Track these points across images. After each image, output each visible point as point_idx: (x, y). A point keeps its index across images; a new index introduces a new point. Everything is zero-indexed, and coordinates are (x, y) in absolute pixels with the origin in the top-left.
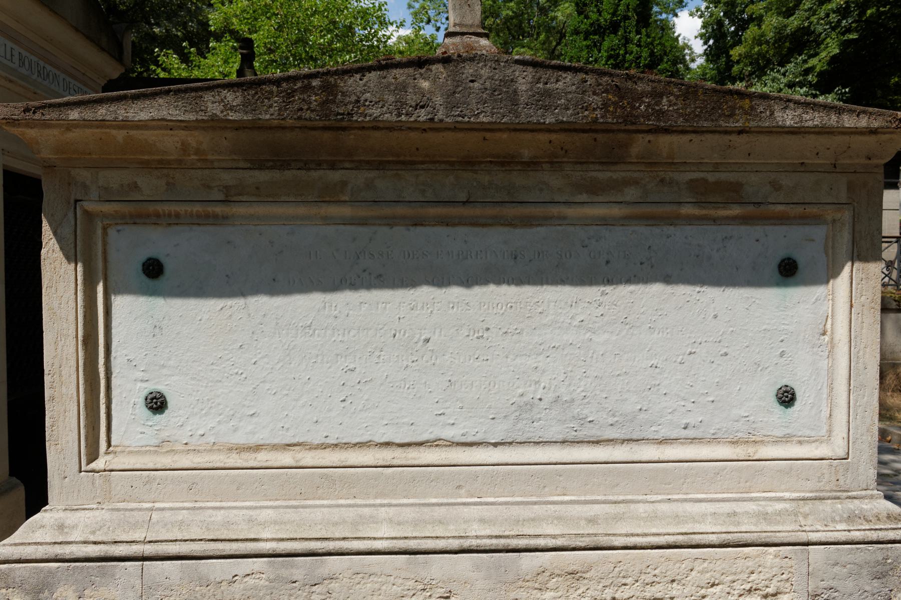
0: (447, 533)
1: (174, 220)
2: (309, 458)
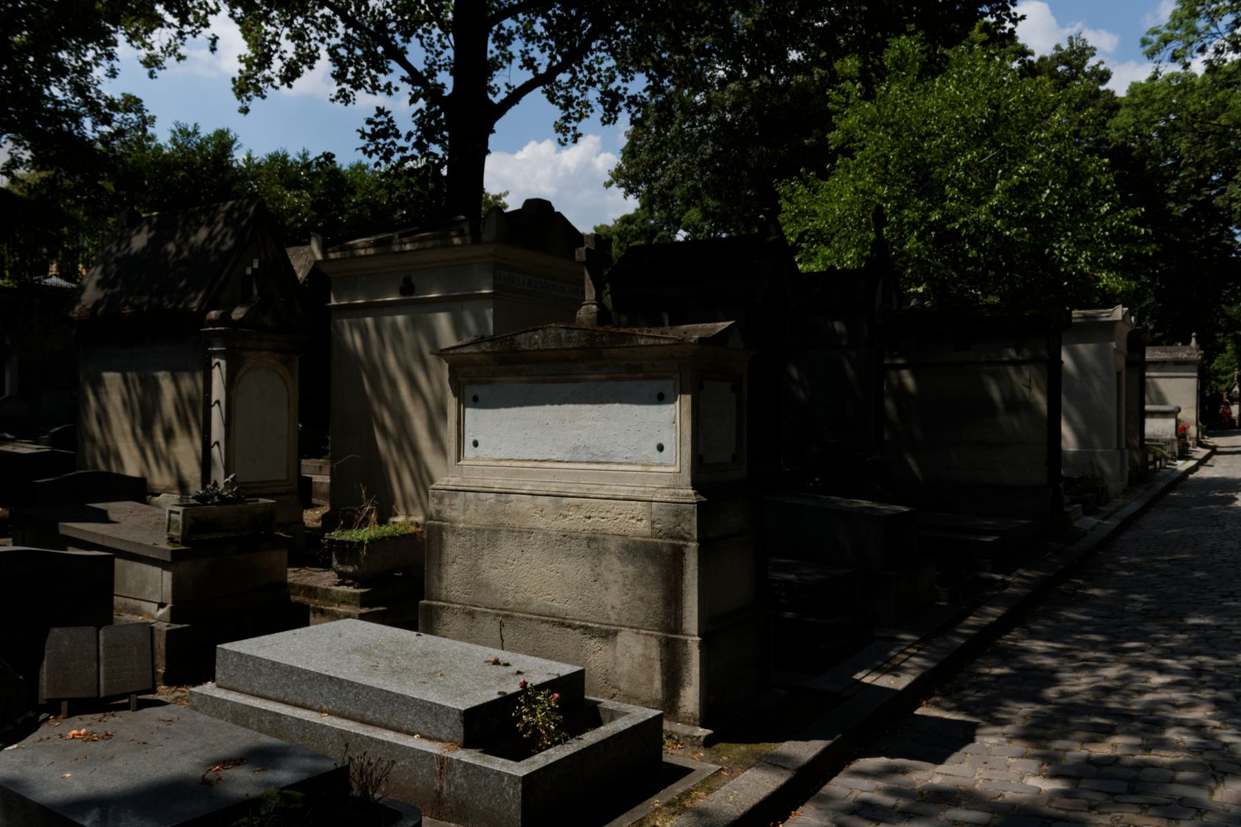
0: (543, 490)
2: (514, 464)
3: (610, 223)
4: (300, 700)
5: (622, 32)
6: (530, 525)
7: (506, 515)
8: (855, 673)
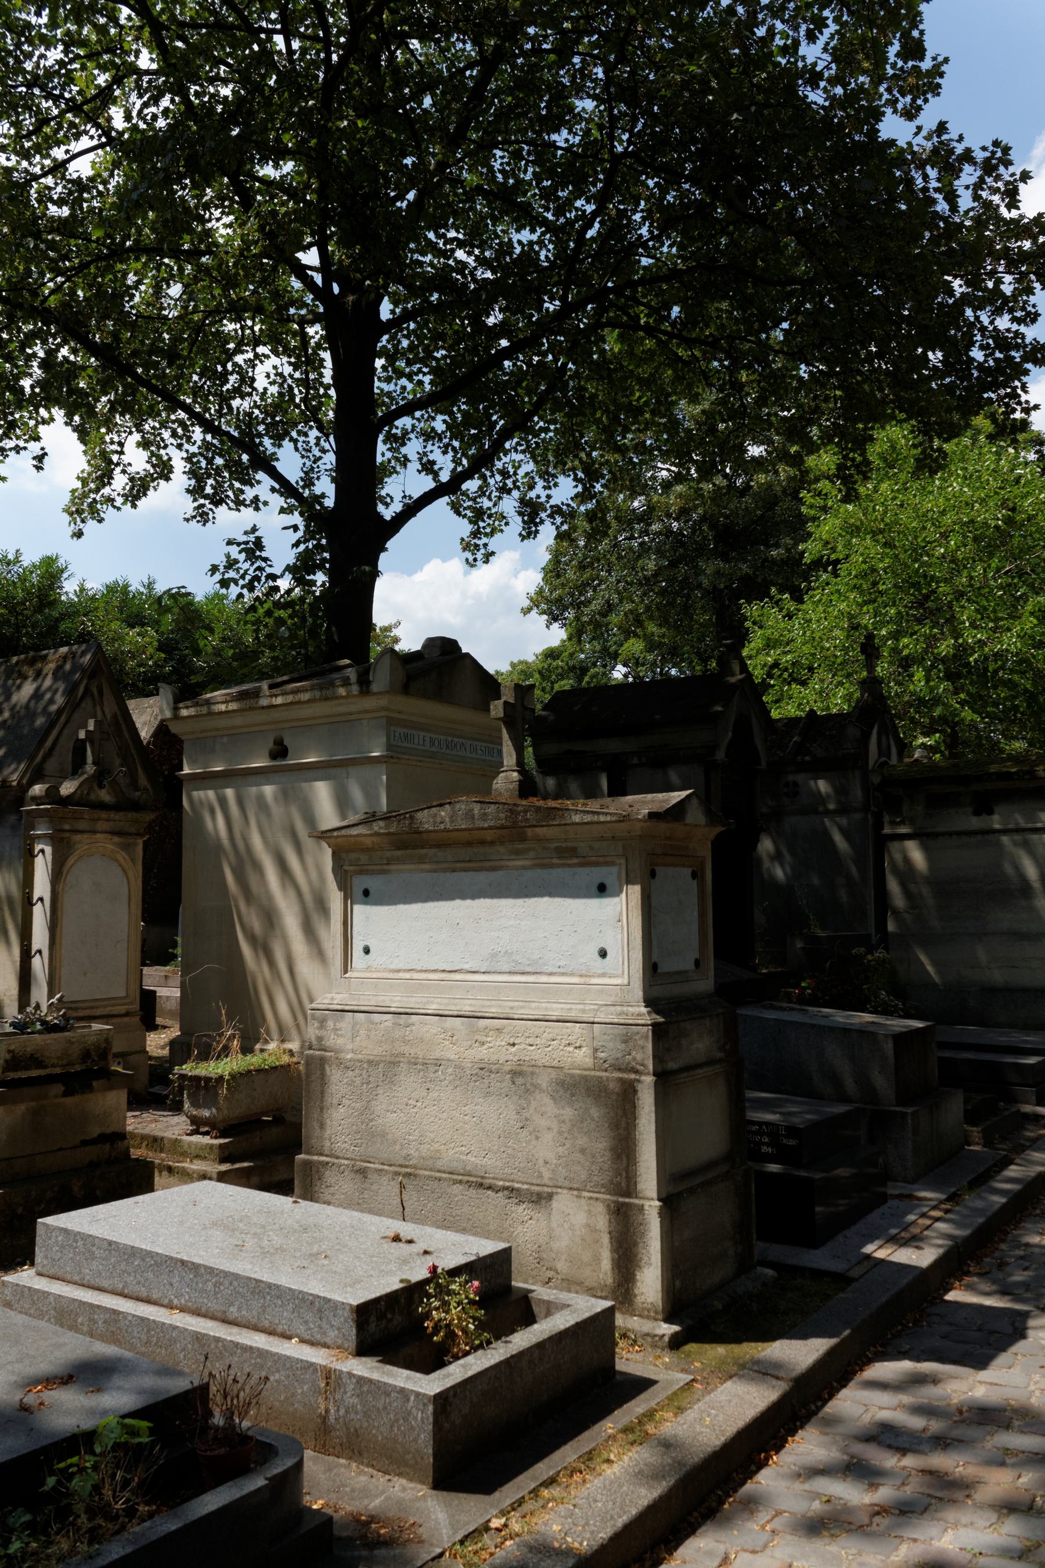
1: (372, 873)
2: (416, 976)
3: (531, 659)
4: (144, 1293)
5: (542, 430)
6: (437, 1054)
7: (406, 1042)
8: (864, 1245)
